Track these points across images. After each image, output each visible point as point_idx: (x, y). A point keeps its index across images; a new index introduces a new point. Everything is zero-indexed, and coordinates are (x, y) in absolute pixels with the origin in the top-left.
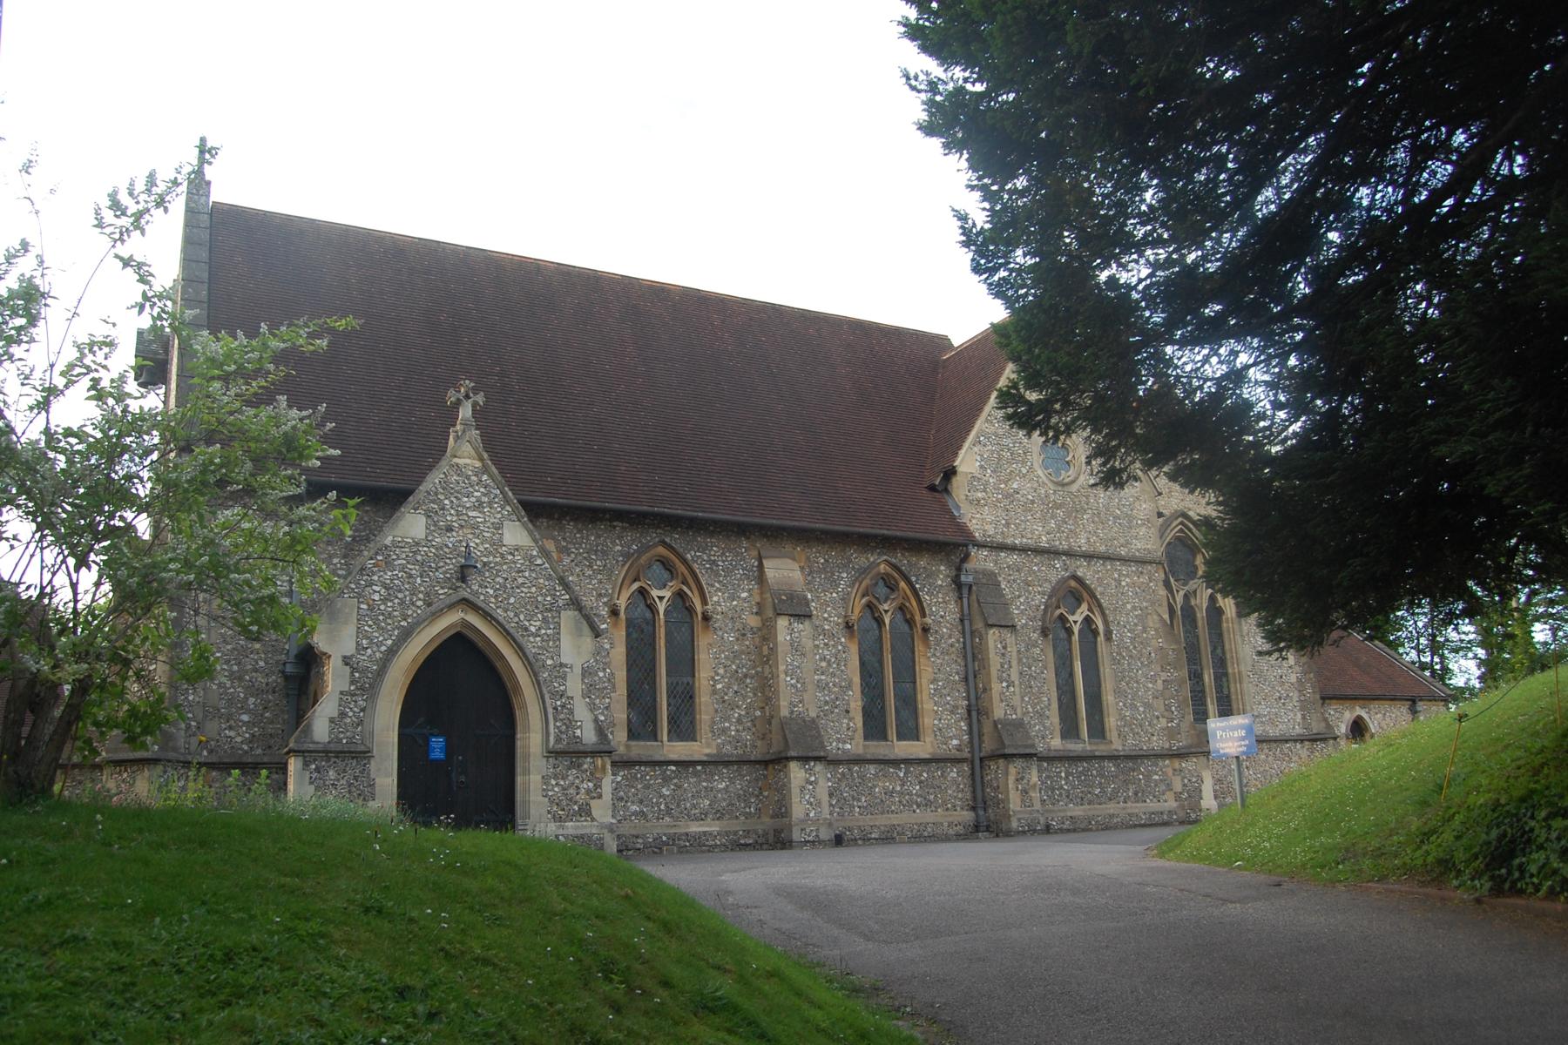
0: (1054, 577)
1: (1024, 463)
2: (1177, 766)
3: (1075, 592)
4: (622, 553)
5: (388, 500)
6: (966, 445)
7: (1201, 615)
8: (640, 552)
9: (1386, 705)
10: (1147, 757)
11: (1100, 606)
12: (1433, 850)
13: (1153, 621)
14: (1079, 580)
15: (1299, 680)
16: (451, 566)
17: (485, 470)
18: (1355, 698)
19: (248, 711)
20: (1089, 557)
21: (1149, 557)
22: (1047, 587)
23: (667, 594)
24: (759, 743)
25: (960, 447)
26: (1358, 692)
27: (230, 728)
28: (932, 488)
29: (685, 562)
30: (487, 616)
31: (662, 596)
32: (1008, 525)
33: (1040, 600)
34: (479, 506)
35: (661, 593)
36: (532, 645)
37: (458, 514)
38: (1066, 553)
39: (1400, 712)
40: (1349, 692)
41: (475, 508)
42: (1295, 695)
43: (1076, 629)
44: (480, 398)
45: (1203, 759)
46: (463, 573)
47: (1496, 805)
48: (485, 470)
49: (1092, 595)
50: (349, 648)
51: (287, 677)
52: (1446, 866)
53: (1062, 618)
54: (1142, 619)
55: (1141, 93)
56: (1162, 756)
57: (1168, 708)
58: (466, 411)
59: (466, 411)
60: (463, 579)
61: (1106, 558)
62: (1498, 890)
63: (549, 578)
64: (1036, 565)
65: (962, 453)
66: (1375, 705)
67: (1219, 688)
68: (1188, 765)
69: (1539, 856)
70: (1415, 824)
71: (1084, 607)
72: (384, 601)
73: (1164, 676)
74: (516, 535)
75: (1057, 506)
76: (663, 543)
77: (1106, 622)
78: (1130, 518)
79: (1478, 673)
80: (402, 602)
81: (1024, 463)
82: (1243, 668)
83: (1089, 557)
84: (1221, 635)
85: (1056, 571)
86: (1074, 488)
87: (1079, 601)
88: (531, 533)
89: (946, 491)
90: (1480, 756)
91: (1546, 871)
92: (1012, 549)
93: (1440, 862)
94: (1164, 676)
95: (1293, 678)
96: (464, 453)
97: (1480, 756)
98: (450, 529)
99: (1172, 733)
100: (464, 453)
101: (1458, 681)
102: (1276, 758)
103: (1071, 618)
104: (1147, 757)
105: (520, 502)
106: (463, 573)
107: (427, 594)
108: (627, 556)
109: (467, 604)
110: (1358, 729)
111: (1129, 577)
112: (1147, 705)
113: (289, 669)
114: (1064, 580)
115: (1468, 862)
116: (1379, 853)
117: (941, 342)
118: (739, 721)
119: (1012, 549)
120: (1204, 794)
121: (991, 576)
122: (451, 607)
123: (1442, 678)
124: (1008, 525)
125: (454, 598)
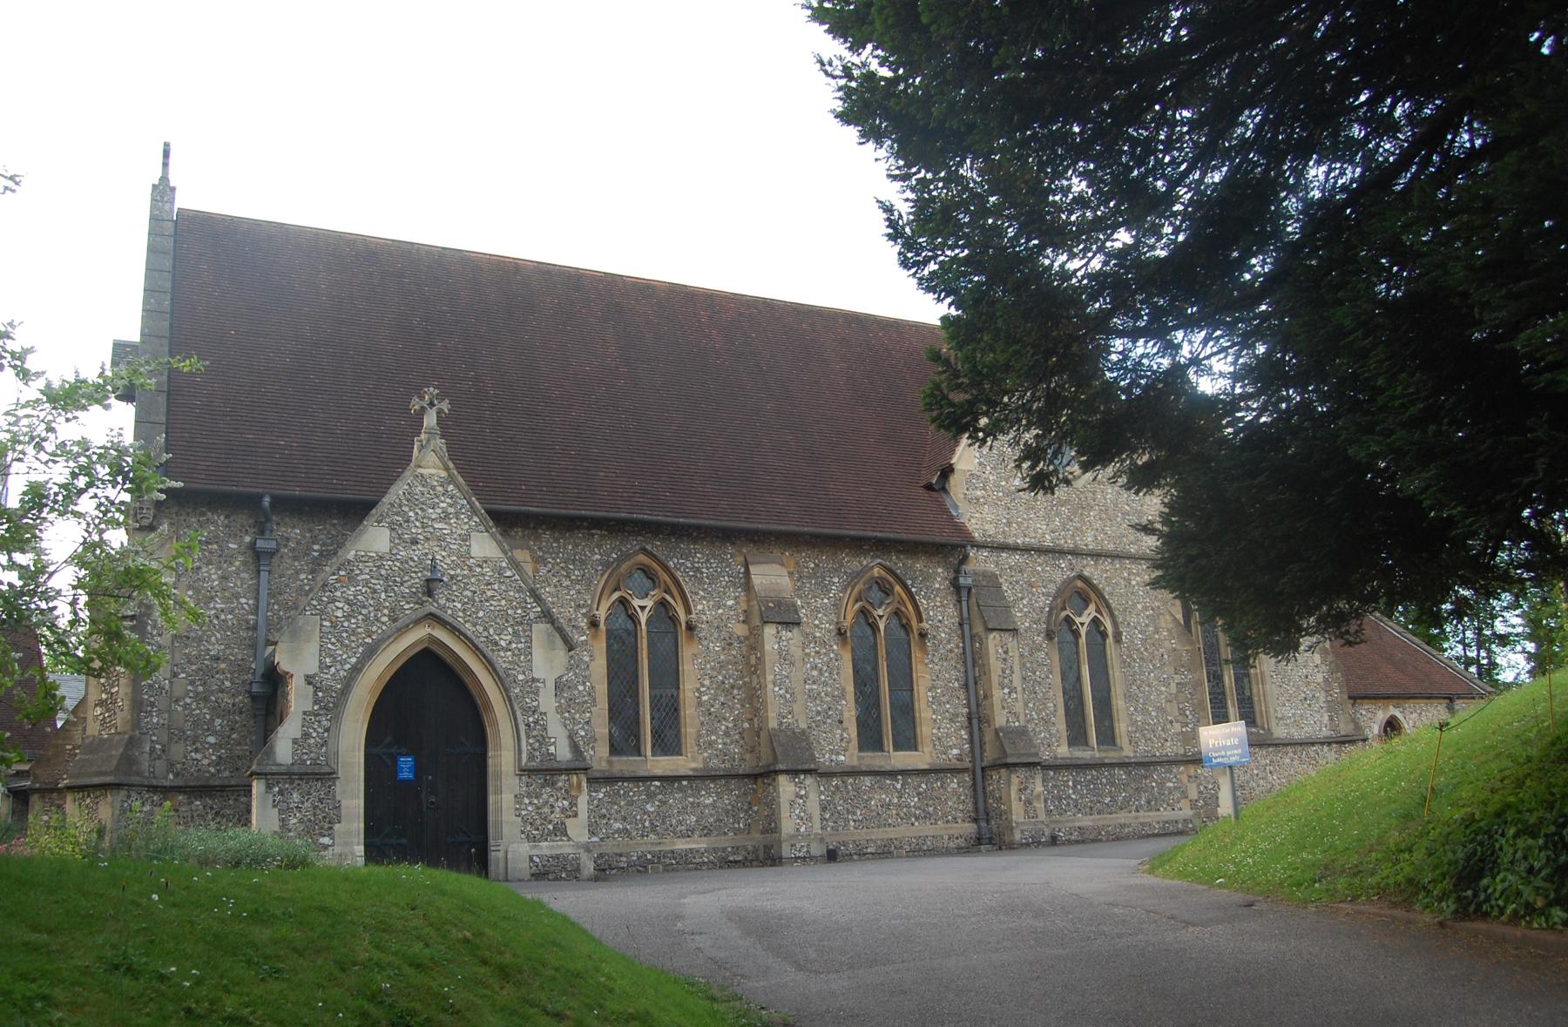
0: (1059, 577)
2: (1192, 772)
4: (601, 562)
8: (620, 561)
9: (1422, 703)
10: (1160, 763)
11: (1108, 606)
14: (1081, 577)
16: (417, 580)
17: (451, 480)
18: (1388, 697)
19: (215, 733)
20: (1096, 555)
22: (1052, 588)
24: (747, 756)
27: (197, 750)
28: (929, 487)
29: (666, 569)
30: (455, 631)
31: (643, 605)
32: (1009, 524)
33: (1044, 602)
34: (445, 517)
35: (642, 603)
36: (502, 660)
38: (1070, 552)
40: (1382, 691)
41: (441, 520)
42: (1321, 696)
43: (1083, 631)
46: (429, 587)
48: (451, 480)
49: (1100, 595)
50: (312, 667)
51: (253, 697)
54: (1154, 619)
56: (1177, 763)
57: (1182, 712)
58: (430, 420)
59: (430, 420)
60: (430, 593)
62: (1462, 913)
64: (1040, 565)
66: (1409, 704)
70: (1394, 837)
71: (1092, 607)
72: (348, 617)
73: (1178, 679)
74: (484, 546)
76: (644, 551)
77: (1115, 624)
79: (1528, 667)
80: (367, 618)
83: (1096, 555)
85: (1061, 571)
88: (499, 544)
89: (944, 490)
90: (1471, 766)
92: (1014, 549)
94: (1178, 679)
95: (1320, 678)
96: (430, 463)
98: (415, 542)
100: (430, 463)
103: (1078, 620)
104: (1160, 763)
105: (489, 512)
106: (429, 587)
107: (393, 610)
108: (607, 565)
109: (434, 618)
112: (1161, 710)
114: (1070, 581)
116: (1357, 872)
118: (727, 734)
119: (1014, 549)
122: (417, 622)
124: (1009, 524)
125: (421, 612)
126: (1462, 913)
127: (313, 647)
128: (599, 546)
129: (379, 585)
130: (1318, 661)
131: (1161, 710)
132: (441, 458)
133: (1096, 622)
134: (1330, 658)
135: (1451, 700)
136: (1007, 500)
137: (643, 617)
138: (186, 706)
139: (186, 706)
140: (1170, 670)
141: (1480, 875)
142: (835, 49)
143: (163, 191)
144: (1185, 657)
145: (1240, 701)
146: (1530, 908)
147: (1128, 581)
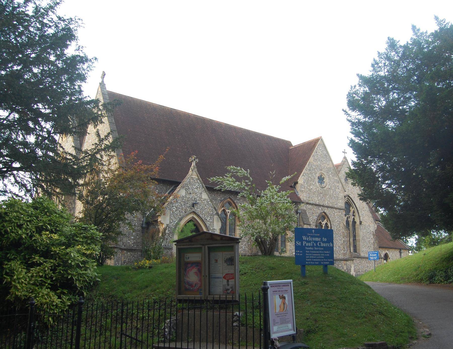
0: (319, 212)
1: (314, 181)
2: (345, 263)
3: (324, 216)
6: (301, 176)
7: (351, 223)
9: (393, 250)
10: (338, 260)
11: (329, 220)
13: (342, 225)
14: (324, 212)
15: (374, 242)
16: (190, 203)
17: (199, 179)
18: (386, 248)
19: (133, 236)
20: (328, 207)
22: (317, 215)
23: (230, 211)
24: (249, 251)
25: (299, 176)
26: (387, 246)
27: (129, 240)
28: (291, 187)
30: (198, 216)
31: (229, 211)
32: (309, 198)
33: (315, 218)
34: (197, 188)
35: (228, 211)
39: (397, 252)
40: (384, 246)
42: (372, 246)
43: (324, 226)
44: (197, 160)
45: (352, 261)
46: (193, 205)
47: (430, 270)
48: (199, 179)
49: (328, 217)
53: (320, 223)
54: (339, 224)
55: (354, 95)
56: (342, 260)
57: (344, 248)
58: (194, 164)
59: (194, 164)
60: (193, 206)
61: (332, 208)
62: (430, 283)
64: (315, 208)
65: (300, 178)
66: (390, 250)
67: (354, 243)
68: (348, 263)
69: (437, 277)
70: (415, 274)
71: (326, 220)
72: (176, 211)
73: (343, 239)
74: (205, 196)
76: (230, 198)
77: (331, 225)
78: (338, 197)
80: (180, 211)
81: (314, 181)
82: (360, 238)
83: (328, 207)
84: (355, 229)
85: (319, 211)
86: (325, 189)
88: (208, 196)
89: (295, 188)
90: (426, 262)
91: (438, 280)
92: (310, 204)
93: (420, 279)
94: (343, 239)
95: (372, 242)
96: (193, 174)
97: (426, 262)
98: (190, 194)
99: (344, 254)
100: (193, 174)
101: (410, 244)
103: (323, 223)
104: (338, 260)
106: (193, 205)
107: (185, 210)
108: (221, 201)
109: (194, 213)
110: (386, 257)
111: (336, 212)
112: (339, 247)
114: (321, 213)
115: (425, 279)
116: (408, 278)
117: (288, 144)
118: (245, 245)
119: (310, 204)
121: (305, 211)
122: (190, 213)
123: (405, 243)
124: (309, 198)
127: (168, 218)
128: (220, 196)
129: (183, 203)
130: (372, 237)
132: (197, 174)
134: (375, 237)
135: (401, 250)
136: (309, 191)
142: (352, 136)
144: (346, 234)
145: (354, 246)
146: (441, 281)
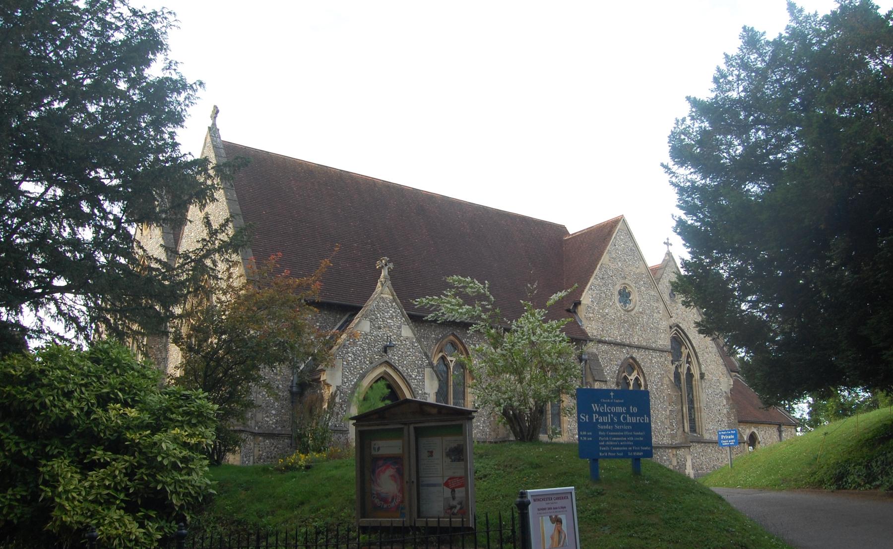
0: (623, 357)
1: (611, 300)
3: (632, 365)
4: (435, 338)
5: (351, 310)
6: (586, 290)
7: (683, 377)
8: (443, 338)
9: (766, 427)
10: (661, 448)
12: (818, 477)
13: (666, 381)
14: (632, 358)
15: (728, 412)
16: (380, 345)
17: (394, 300)
18: (752, 423)
19: (275, 409)
20: (638, 348)
21: (665, 349)
22: (620, 362)
23: (454, 359)
25: (583, 291)
28: (569, 311)
29: (462, 343)
30: (395, 369)
32: (603, 331)
33: (616, 368)
34: (391, 318)
35: (452, 359)
36: (413, 383)
37: (383, 321)
38: (628, 346)
39: (773, 431)
40: (749, 419)
41: (390, 318)
42: (725, 420)
43: (632, 383)
44: (391, 265)
45: (687, 450)
46: (386, 349)
47: (838, 463)
48: (394, 300)
50: (339, 383)
51: (292, 393)
52: (821, 482)
53: (625, 378)
54: (661, 379)
57: (671, 424)
58: (384, 273)
59: (384, 273)
60: (386, 352)
61: (646, 348)
62: (838, 489)
63: (420, 352)
64: (615, 351)
65: (584, 294)
67: (690, 414)
68: (680, 452)
69: (852, 477)
71: (635, 372)
72: (353, 361)
74: (407, 332)
75: (625, 322)
76: (453, 335)
77: (645, 380)
78: (657, 329)
79: (808, 411)
80: (360, 362)
83: (638, 348)
84: (691, 388)
85: (623, 355)
86: (633, 313)
87: (633, 370)
89: (575, 312)
90: (830, 448)
91: (854, 481)
92: (605, 342)
95: (725, 411)
96: (383, 292)
97: (830, 448)
98: (380, 328)
99: (673, 436)
100: (383, 292)
101: (797, 415)
102: (716, 451)
104: (661, 448)
105: (409, 315)
106: (386, 349)
107: (371, 358)
108: (438, 340)
109: (387, 363)
110: (753, 440)
111: (656, 358)
112: (662, 422)
113: (295, 389)
114: (627, 359)
116: (796, 480)
117: (561, 230)
118: (484, 422)
119: (605, 342)
120: (687, 467)
121: (596, 356)
122: (381, 364)
123: (789, 412)
124: (603, 331)
125: (383, 360)
126: (838, 489)
127: (339, 374)
129: (365, 347)
131: (662, 422)
133: (637, 379)
134: (731, 402)
135: (780, 426)
137: (452, 365)
138: (263, 396)
139: (263, 396)
140: (667, 404)
141: (843, 478)
143: (213, 131)
144: (674, 398)
146: (859, 485)
147: (651, 360)
